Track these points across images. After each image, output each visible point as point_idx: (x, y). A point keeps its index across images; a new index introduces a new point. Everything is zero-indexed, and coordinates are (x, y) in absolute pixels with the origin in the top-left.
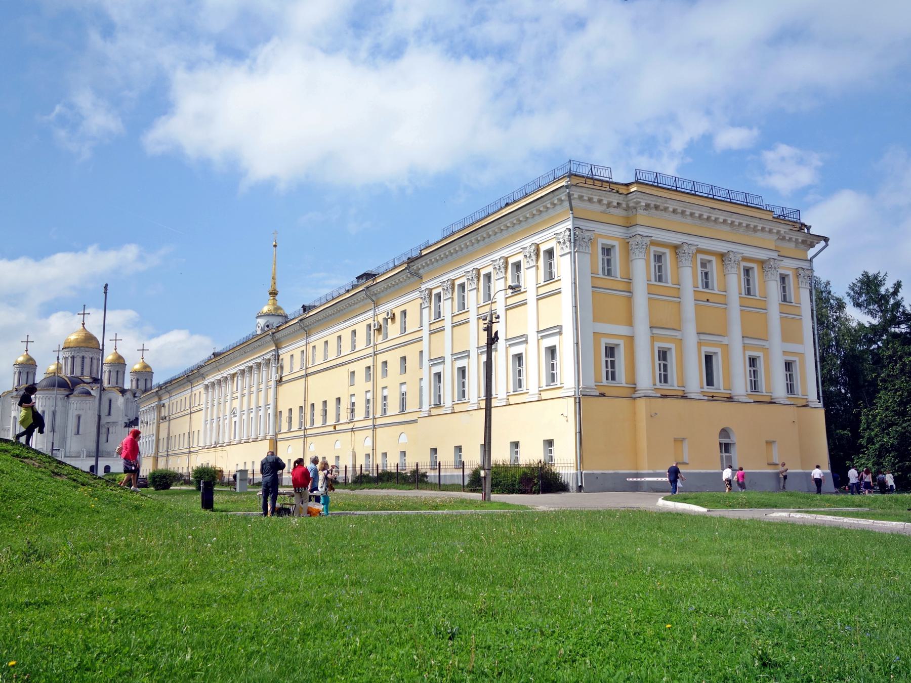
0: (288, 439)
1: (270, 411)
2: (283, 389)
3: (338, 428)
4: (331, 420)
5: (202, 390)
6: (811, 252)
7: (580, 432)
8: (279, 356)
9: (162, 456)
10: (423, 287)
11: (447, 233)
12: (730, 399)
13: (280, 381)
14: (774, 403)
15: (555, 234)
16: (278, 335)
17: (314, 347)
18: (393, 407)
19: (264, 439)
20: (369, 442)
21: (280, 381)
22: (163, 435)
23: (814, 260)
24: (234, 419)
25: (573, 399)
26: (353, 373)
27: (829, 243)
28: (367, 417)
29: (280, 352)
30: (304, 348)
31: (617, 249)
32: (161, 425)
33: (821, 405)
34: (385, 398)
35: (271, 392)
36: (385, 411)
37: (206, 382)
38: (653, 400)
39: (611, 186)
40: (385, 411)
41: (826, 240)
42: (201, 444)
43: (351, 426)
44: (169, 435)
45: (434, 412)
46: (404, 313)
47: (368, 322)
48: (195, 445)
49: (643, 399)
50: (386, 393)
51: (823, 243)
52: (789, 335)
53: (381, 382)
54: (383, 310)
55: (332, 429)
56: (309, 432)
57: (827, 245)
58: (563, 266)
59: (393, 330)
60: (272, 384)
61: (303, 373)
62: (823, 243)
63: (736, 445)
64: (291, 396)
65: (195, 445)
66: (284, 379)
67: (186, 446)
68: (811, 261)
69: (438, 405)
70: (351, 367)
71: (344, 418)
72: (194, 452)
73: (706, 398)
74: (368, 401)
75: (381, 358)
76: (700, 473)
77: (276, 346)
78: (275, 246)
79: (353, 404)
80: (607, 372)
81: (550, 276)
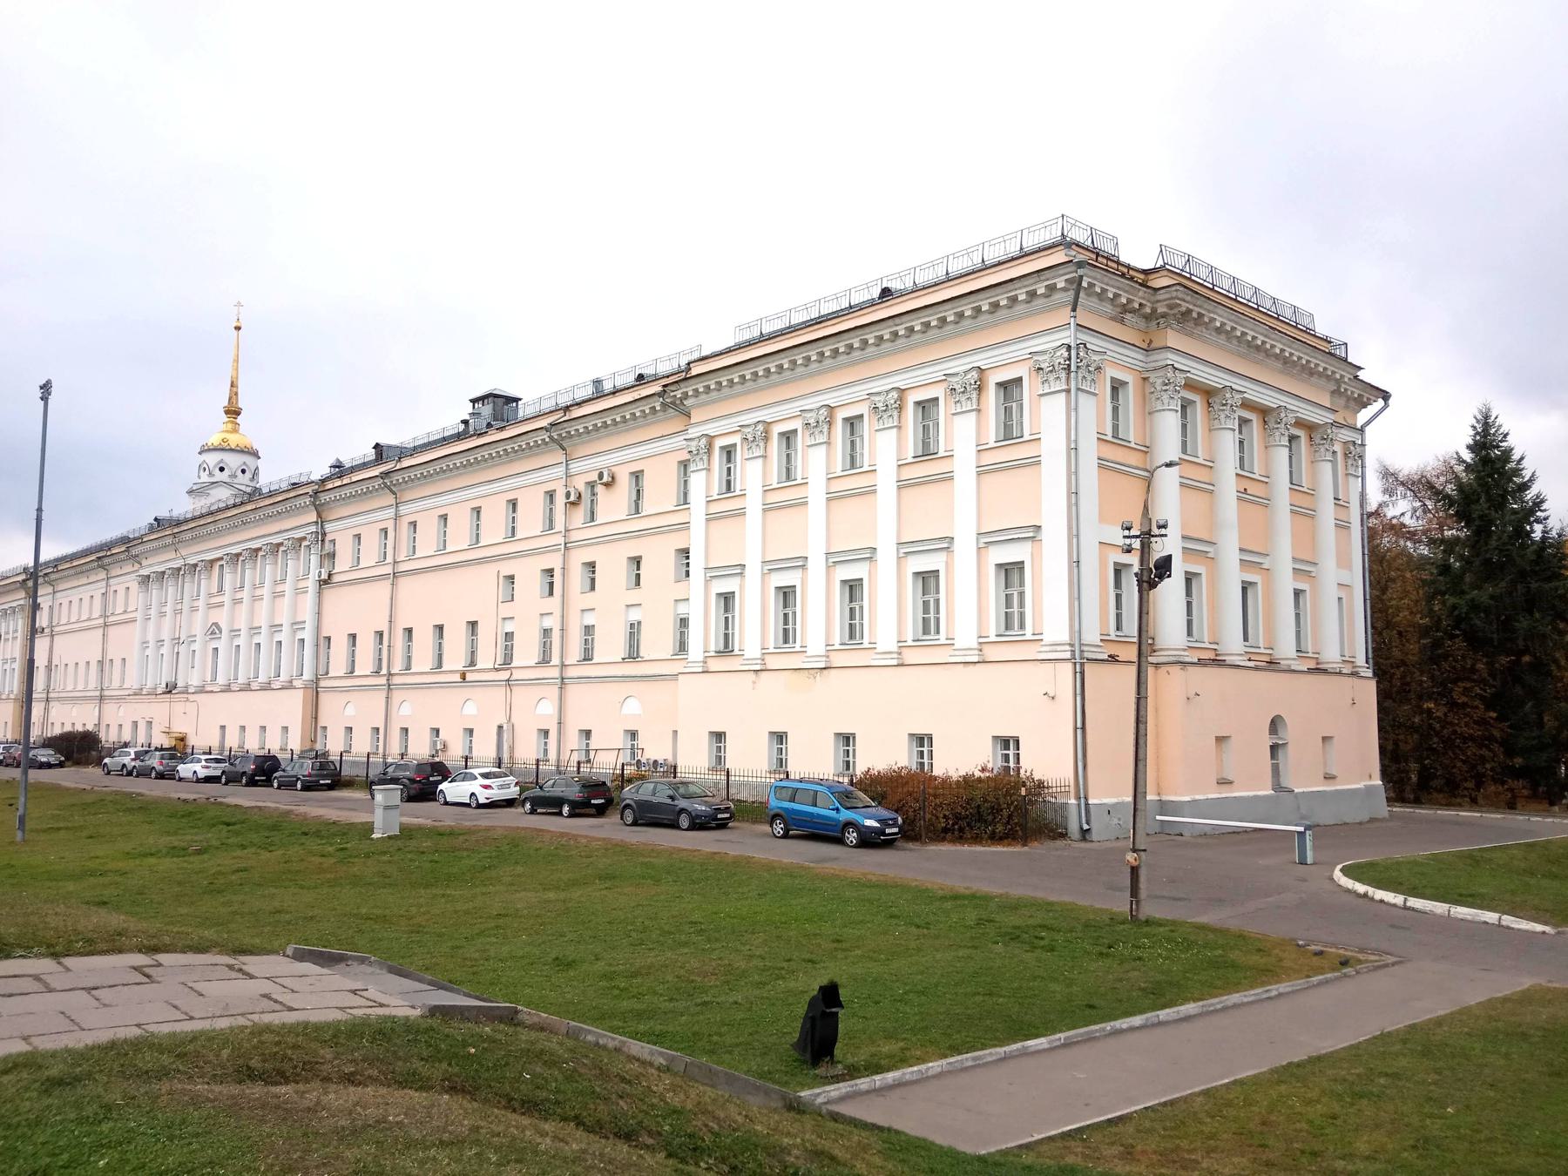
0: (348, 690)
1: (307, 634)
2: (330, 594)
3: (469, 677)
4: (455, 659)
5: (134, 586)
6: (1363, 416)
7: (1083, 728)
8: (324, 534)
9: (40, 700)
10: (694, 432)
11: (747, 336)
12: (1272, 665)
13: (325, 582)
14: (1325, 671)
15: (1016, 348)
16: (324, 497)
17: (414, 524)
18: (610, 647)
19: (289, 686)
20: (548, 708)
21: (325, 582)
22: (40, 660)
23: (1367, 429)
24: (214, 644)
25: (1069, 666)
26: (511, 578)
27: (1391, 401)
28: (545, 660)
29: (328, 527)
30: (390, 525)
31: (1131, 386)
32: (37, 642)
33: (1370, 674)
34: (589, 630)
35: (309, 600)
36: (587, 657)
37: (145, 572)
38: (1191, 669)
39: (1126, 273)
40: (587, 657)
41: (1386, 396)
42: (132, 682)
43: (504, 675)
44: (50, 661)
45: (715, 665)
46: (637, 476)
47: (549, 487)
48: (116, 684)
49: (1176, 669)
50: (589, 619)
51: (1381, 403)
52: (1343, 562)
53: (578, 599)
54: (585, 469)
55: (457, 678)
56: (111, 619)
57: (1386, 406)
58: (1047, 415)
59: (613, 505)
60: (311, 584)
61: (388, 570)
62: (1381, 403)
63: (1290, 747)
64: (356, 611)
65: (116, 684)
66: (336, 579)
67: (93, 684)
68: (1362, 430)
69: (726, 650)
70: (507, 568)
71: (485, 660)
72: (111, 697)
73: (1251, 664)
74: (547, 632)
75: (579, 557)
76: (1256, 797)
77: (319, 515)
78: (238, 328)
79: (509, 636)
80: (1022, 604)
81: (1009, 432)
